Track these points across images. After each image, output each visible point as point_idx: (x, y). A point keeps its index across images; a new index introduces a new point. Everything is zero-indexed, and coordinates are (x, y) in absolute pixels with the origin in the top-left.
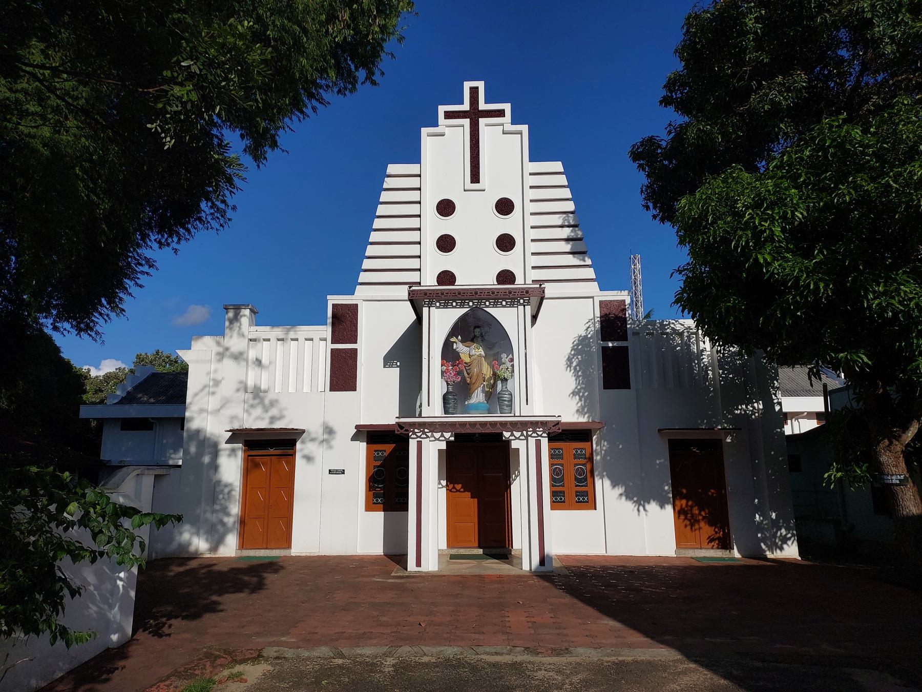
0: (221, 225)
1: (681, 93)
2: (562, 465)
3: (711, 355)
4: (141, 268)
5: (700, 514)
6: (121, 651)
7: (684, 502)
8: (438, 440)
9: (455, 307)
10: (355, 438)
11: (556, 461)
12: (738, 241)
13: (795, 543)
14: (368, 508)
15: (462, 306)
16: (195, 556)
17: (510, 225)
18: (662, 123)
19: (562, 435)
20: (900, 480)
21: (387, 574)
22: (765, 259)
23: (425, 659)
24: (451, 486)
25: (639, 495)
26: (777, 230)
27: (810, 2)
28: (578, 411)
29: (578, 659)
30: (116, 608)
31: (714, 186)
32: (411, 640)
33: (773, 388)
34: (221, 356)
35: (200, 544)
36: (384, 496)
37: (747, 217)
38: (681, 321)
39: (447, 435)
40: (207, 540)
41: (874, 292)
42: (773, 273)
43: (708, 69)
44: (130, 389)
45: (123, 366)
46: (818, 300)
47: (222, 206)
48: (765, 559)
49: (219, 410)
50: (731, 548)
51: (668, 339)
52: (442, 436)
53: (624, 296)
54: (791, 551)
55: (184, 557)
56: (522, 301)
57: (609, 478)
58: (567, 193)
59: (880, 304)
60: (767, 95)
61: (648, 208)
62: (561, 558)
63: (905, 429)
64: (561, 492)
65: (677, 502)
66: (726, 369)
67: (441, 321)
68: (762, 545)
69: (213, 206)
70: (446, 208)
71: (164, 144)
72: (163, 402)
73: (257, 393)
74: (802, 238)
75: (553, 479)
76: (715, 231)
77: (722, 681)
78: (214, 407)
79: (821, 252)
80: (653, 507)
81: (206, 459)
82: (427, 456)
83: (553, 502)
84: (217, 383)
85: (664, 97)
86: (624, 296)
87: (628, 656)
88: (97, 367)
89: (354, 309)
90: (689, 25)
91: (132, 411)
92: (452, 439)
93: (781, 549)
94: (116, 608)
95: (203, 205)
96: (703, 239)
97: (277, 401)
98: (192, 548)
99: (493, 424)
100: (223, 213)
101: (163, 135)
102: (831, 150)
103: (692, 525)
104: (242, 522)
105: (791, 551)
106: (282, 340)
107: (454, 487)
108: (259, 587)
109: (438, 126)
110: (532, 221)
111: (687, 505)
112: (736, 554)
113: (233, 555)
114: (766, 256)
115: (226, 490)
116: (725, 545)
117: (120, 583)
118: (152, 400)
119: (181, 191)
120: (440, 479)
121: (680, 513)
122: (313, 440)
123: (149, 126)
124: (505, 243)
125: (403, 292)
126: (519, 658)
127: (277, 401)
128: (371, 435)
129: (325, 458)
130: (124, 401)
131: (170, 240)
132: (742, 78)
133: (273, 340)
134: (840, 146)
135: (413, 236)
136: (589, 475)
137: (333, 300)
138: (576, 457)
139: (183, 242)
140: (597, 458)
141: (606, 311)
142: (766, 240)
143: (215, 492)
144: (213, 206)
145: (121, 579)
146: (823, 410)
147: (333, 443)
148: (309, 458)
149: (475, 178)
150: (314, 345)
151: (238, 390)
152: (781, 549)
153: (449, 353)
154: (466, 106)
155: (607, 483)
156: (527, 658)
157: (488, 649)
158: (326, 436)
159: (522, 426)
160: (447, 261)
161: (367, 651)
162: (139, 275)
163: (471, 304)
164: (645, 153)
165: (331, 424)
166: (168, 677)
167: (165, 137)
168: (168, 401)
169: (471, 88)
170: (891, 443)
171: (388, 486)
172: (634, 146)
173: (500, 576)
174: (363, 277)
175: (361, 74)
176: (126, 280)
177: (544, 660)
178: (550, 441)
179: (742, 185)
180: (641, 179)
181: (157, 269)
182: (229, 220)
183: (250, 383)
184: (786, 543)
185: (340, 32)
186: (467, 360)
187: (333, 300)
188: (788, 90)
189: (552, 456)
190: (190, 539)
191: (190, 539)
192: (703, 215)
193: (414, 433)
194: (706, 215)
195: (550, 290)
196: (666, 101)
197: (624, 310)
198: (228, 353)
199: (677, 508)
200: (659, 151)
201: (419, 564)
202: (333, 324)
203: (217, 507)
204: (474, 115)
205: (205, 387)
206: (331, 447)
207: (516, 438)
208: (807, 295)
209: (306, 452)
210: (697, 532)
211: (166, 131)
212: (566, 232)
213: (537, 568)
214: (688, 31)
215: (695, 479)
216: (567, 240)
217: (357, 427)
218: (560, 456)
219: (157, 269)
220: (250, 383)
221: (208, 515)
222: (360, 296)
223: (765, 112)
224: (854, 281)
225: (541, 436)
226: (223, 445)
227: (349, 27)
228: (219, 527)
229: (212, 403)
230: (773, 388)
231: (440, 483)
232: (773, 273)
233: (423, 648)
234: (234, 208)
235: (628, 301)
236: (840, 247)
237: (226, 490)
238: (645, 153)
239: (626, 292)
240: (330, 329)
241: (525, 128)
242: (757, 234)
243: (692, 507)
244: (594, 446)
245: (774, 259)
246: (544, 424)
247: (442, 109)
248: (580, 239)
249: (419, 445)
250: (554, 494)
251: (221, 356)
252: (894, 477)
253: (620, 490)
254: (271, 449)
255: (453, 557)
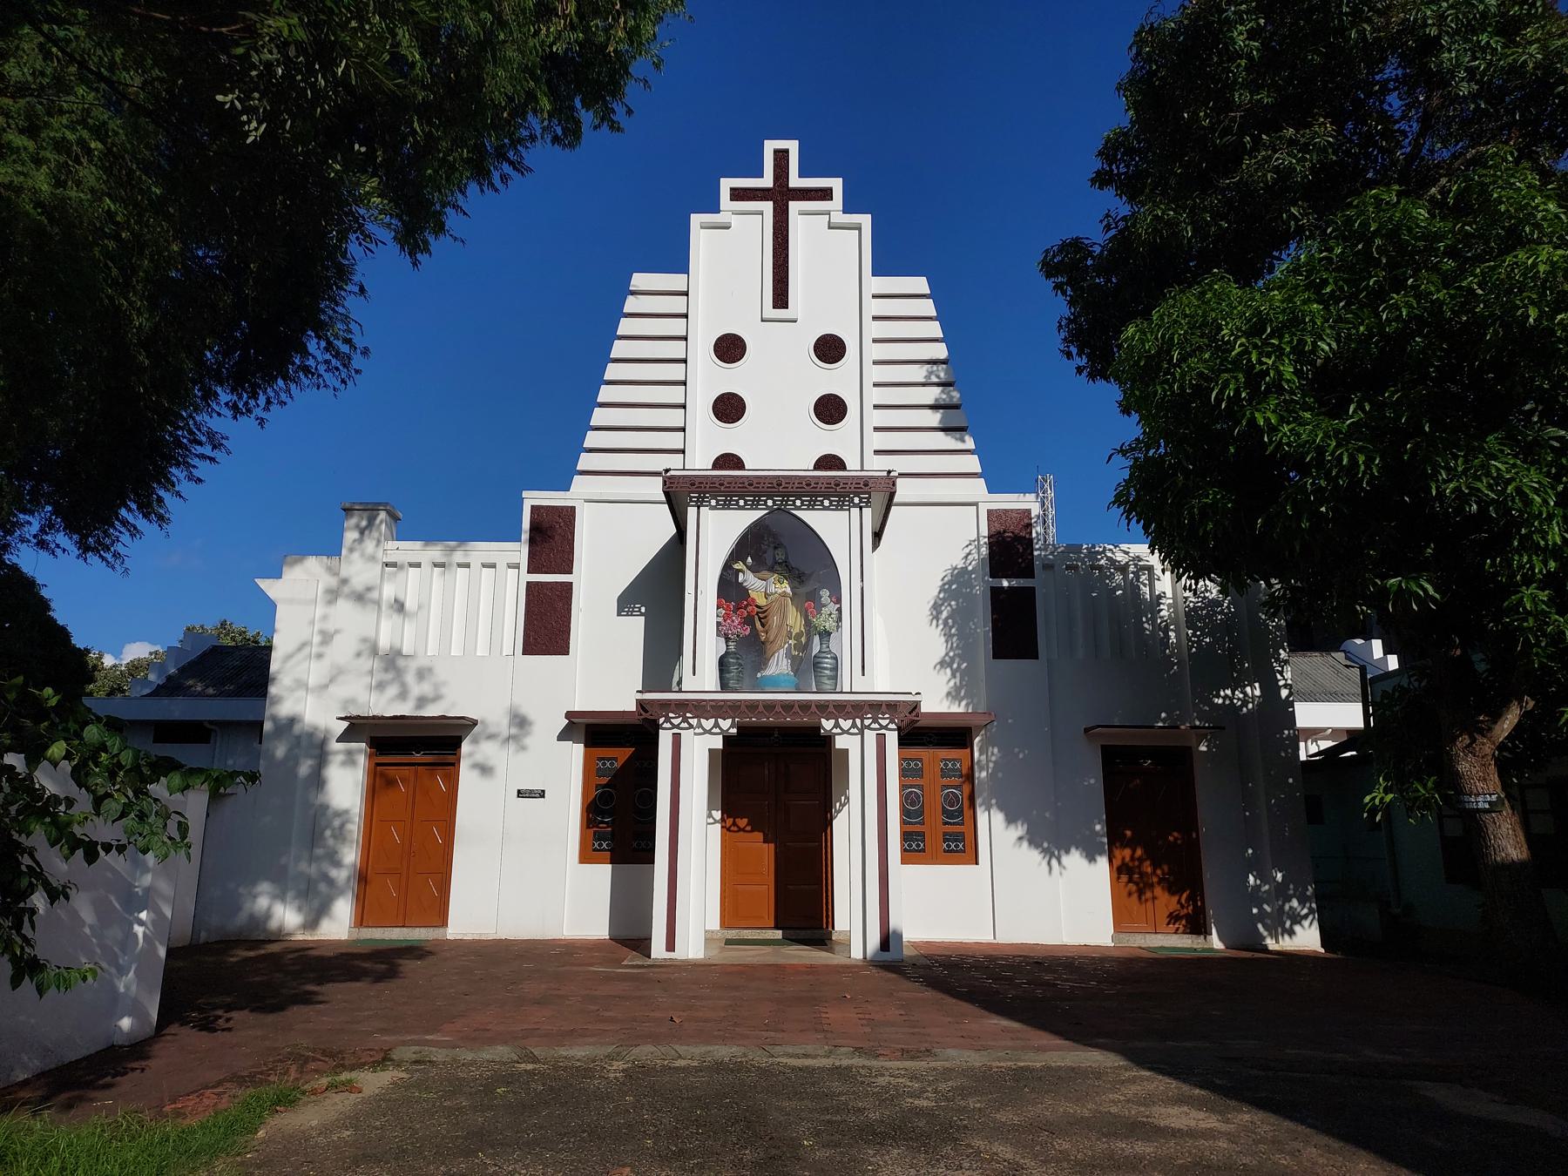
0: (343, 381)
1: (1127, 166)
2: (921, 787)
3: (1174, 605)
4: (199, 450)
5: (1154, 872)
6: (138, 1049)
7: (1127, 852)
8: (709, 732)
9: (742, 508)
10: (564, 736)
11: (910, 781)
12: (1221, 392)
13: (1316, 924)
14: (586, 857)
15: (755, 507)
16: (279, 936)
17: (838, 379)
18: (1093, 216)
19: (920, 733)
20: (1490, 803)
21: (618, 962)
22: (1267, 420)
23: (680, 1063)
24: (730, 821)
25: (1050, 838)
26: (1288, 370)
27: (1339, 6)
28: (949, 694)
29: (947, 1065)
30: (131, 974)
31: (1176, 310)
32: (655, 1039)
33: (1278, 660)
34: (333, 595)
35: (287, 917)
36: (613, 837)
37: (1238, 350)
38: (1124, 547)
39: (725, 724)
40: (300, 909)
41: (1448, 469)
42: (1280, 444)
43: (1174, 119)
44: (173, 671)
45: (158, 648)
46: (1355, 483)
47: (345, 348)
48: (1265, 950)
49: (326, 686)
50: (1207, 933)
51: (1103, 576)
52: (716, 725)
53: (1028, 502)
54: (1307, 938)
55: (258, 937)
56: (856, 500)
57: (1001, 808)
58: (935, 329)
59: (1457, 490)
60: (1268, 159)
61: (1069, 355)
62: (914, 945)
63: (1496, 716)
64: (918, 834)
65: (1117, 853)
66: (1200, 629)
67: (718, 531)
68: (1260, 926)
69: (330, 347)
70: (730, 348)
71: (247, 134)
72: (230, 695)
73: (392, 662)
74: (1328, 386)
75: (905, 812)
76: (1183, 375)
77: (1197, 1091)
78: (319, 680)
79: (1360, 407)
80: (1074, 860)
81: (304, 768)
82: (690, 762)
83: (904, 851)
84: (327, 638)
85: (1098, 173)
86: (1028, 502)
87: (1036, 1061)
88: (117, 654)
89: (568, 515)
90: (1139, 42)
91: (176, 709)
92: (734, 731)
93: (1291, 933)
94: (131, 974)
95: (312, 346)
96: (1164, 390)
97: (430, 670)
98: (273, 924)
99: (805, 706)
100: (346, 361)
101: (245, 118)
102: (1378, 241)
103: (1141, 893)
104: (363, 877)
105: (1307, 938)
106: (442, 565)
107: (734, 824)
108: (392, 973)
109: (718, 211)
110: (876, 374)
111: (1132, 858)
112: (1216, 942)
113: (344, 937)
114: (1269, 414)
115: (337, 823)
116: (1197, 926)
117: (139, 930)
118: (211, 691)
119: (273, 324)
120: (711, 807)
121: (1120, 871)
122: (491, 737)
123: (220, 98)
124: (830, 409)
125: (655, 488)
126: (845, 1062)
127: (430, 670)
128: (592, 731)
129: (516, 769)
130: (158, 692)
131: (252, 403)
132: (1227, 131)
133: (426, 567)
134: (1392, 235)
135: (674, 395)
136: (966, 803)
137: (534, 498)
138: (945, 773)
139: (274, 408)
140: (981, 775)
141: (998, 527)
142: (1268, 391)
143: (318, 826)
144: (330, 347)
145: (141, 923)
146: (1361, 725)
147: (528, 741)
148: (485, 770)
149: (781, 299)
150: (497, 576)
151: (359, 655)
152: (1291, 933)
153: (729, 588)
154: (767, 181)
155: (998, 818)
156: (857, 1061)
157: (790, 1050)
158: (514, 731)
159: (854, 709)
160: (729, 438)
161: (579, 1052)
162: (196, 461)
163: (770, 503)
164: (1066, 264)
165: (527, 710)
166: (219, 1083)
167: (249, 122)
168: (238, 693)
169: (776, 151)
170: (1473, 740)
171: (621, 820)
172: (1047, 251)
173: (811, 966)
174: (586, 461)
175: (586, 117)
176: (173, 470)
177: (888, 1064)
178: (903, 742)
179: (1230, 304)
180: (1060, 307)
181: (229, 453)
182: (357, 372)
183: (384, 643)
184: (1299, 923)
185: (557, 36)
186: (761, 601)
187: (534, 498)
188: (1304, 148)
189: (904, 773)
190: (269, 909)
191: (269, 909)
192: (1165, 350)
193: (668, 720)
194: (1169, 352)
195: (904, 490)
196: (1102, 179)
197: (1029, 526)
198: (346, 589)
199: (1117, 863)
200: (1089, 262)
201: (671, 946)
202: (532, 541)
203: (319, 851)
204: (781, 196)
205: (303, 645)
206: (523, 748)
207: (844, 732)
208: (1337, 476)
209: (479, 758)
210: (1149, 904)
211: (249, 110)
212: (932, 394)
213: (876, 954)
214: (1138, 54)
215: (1146, 811)
216: (934, 407)
217: (569, 715)
218: (918, 773)
219: (229, 453)
220: (384, 643)
221: (303, 866)
222: (578, 493)
223: (1267, 188)
224: (1413, 452)
225: (886, 728)
226: (335, 746)
227: (573, 28)
228: (323, 887)
229: (316, 673)
230: (1278, 660)
231: (710, 816)
232: (1280, 444)
233: (677, 1047)
234: (365, 352)
235: (1036, 510)
236: (1391, 395)
237: (337, 823)
238: (1066, 264)
239: (1032, 497)
240: (525, 550)
241: (865, 220)
242: (1254, 378)
243: (1141, 860)
244: (976, 755)
245: (1282, 420)
246: (892, 707)
247: (726, 184)
248: (956, 407)
249: (677, 740)
250: (906, 836)
251: (333, 595)
252: (1480, 799)
253: (1019, 830)
254: (417, 753)
255: (729, 942)
